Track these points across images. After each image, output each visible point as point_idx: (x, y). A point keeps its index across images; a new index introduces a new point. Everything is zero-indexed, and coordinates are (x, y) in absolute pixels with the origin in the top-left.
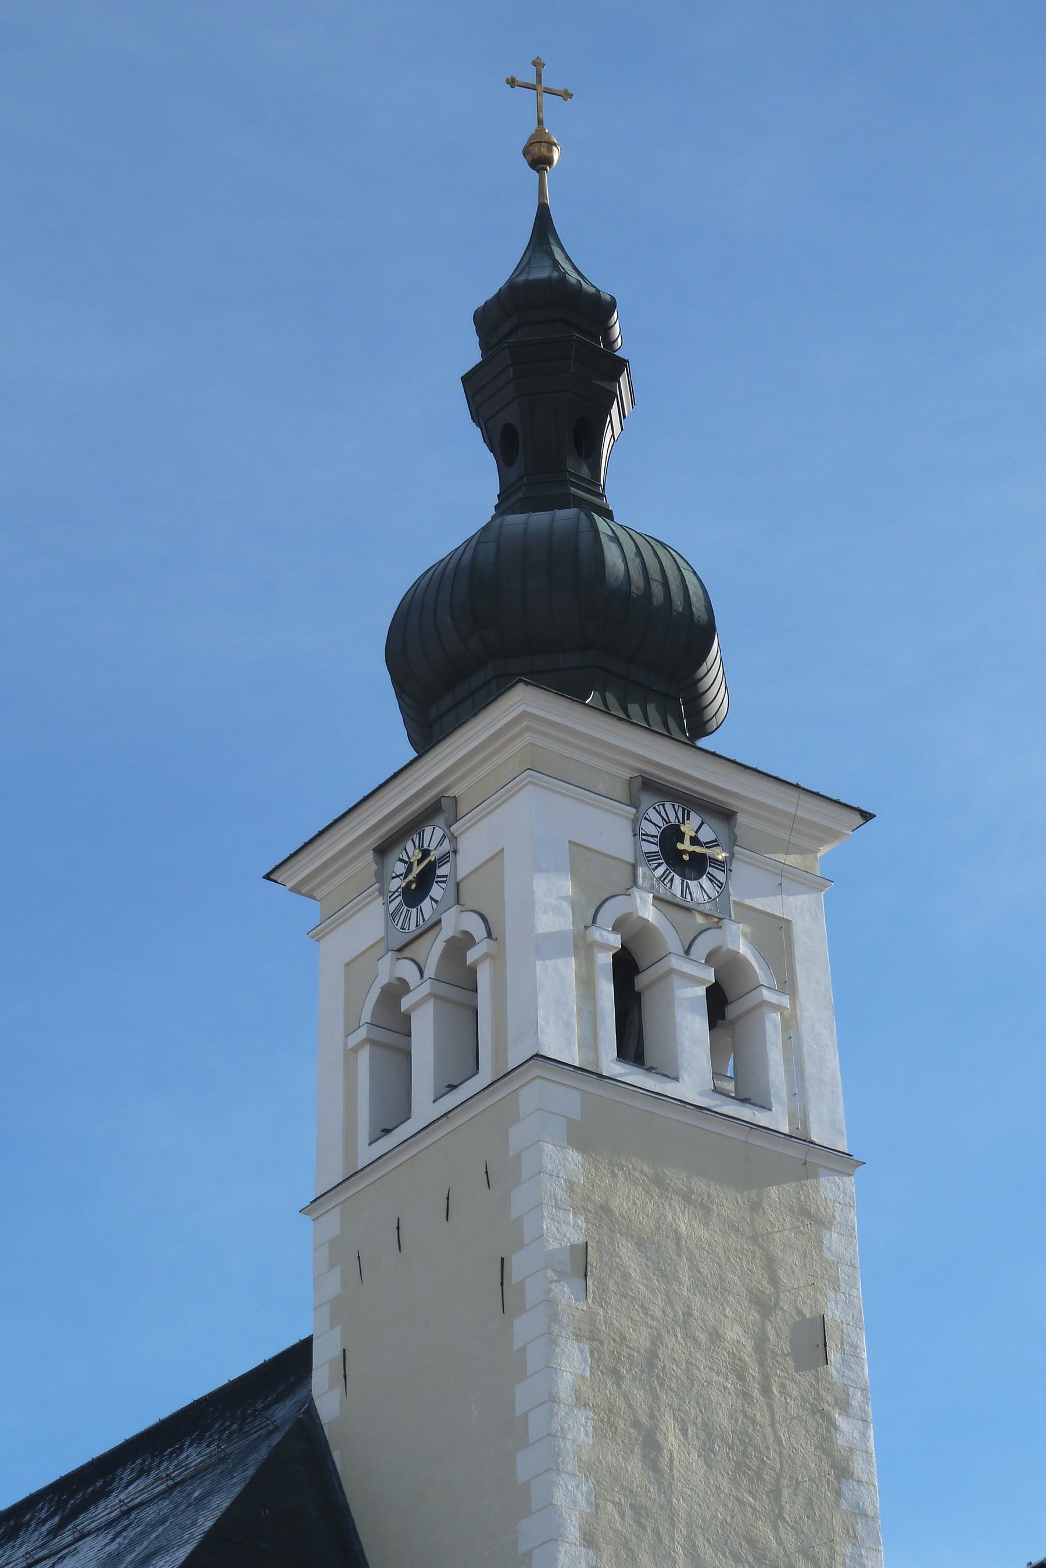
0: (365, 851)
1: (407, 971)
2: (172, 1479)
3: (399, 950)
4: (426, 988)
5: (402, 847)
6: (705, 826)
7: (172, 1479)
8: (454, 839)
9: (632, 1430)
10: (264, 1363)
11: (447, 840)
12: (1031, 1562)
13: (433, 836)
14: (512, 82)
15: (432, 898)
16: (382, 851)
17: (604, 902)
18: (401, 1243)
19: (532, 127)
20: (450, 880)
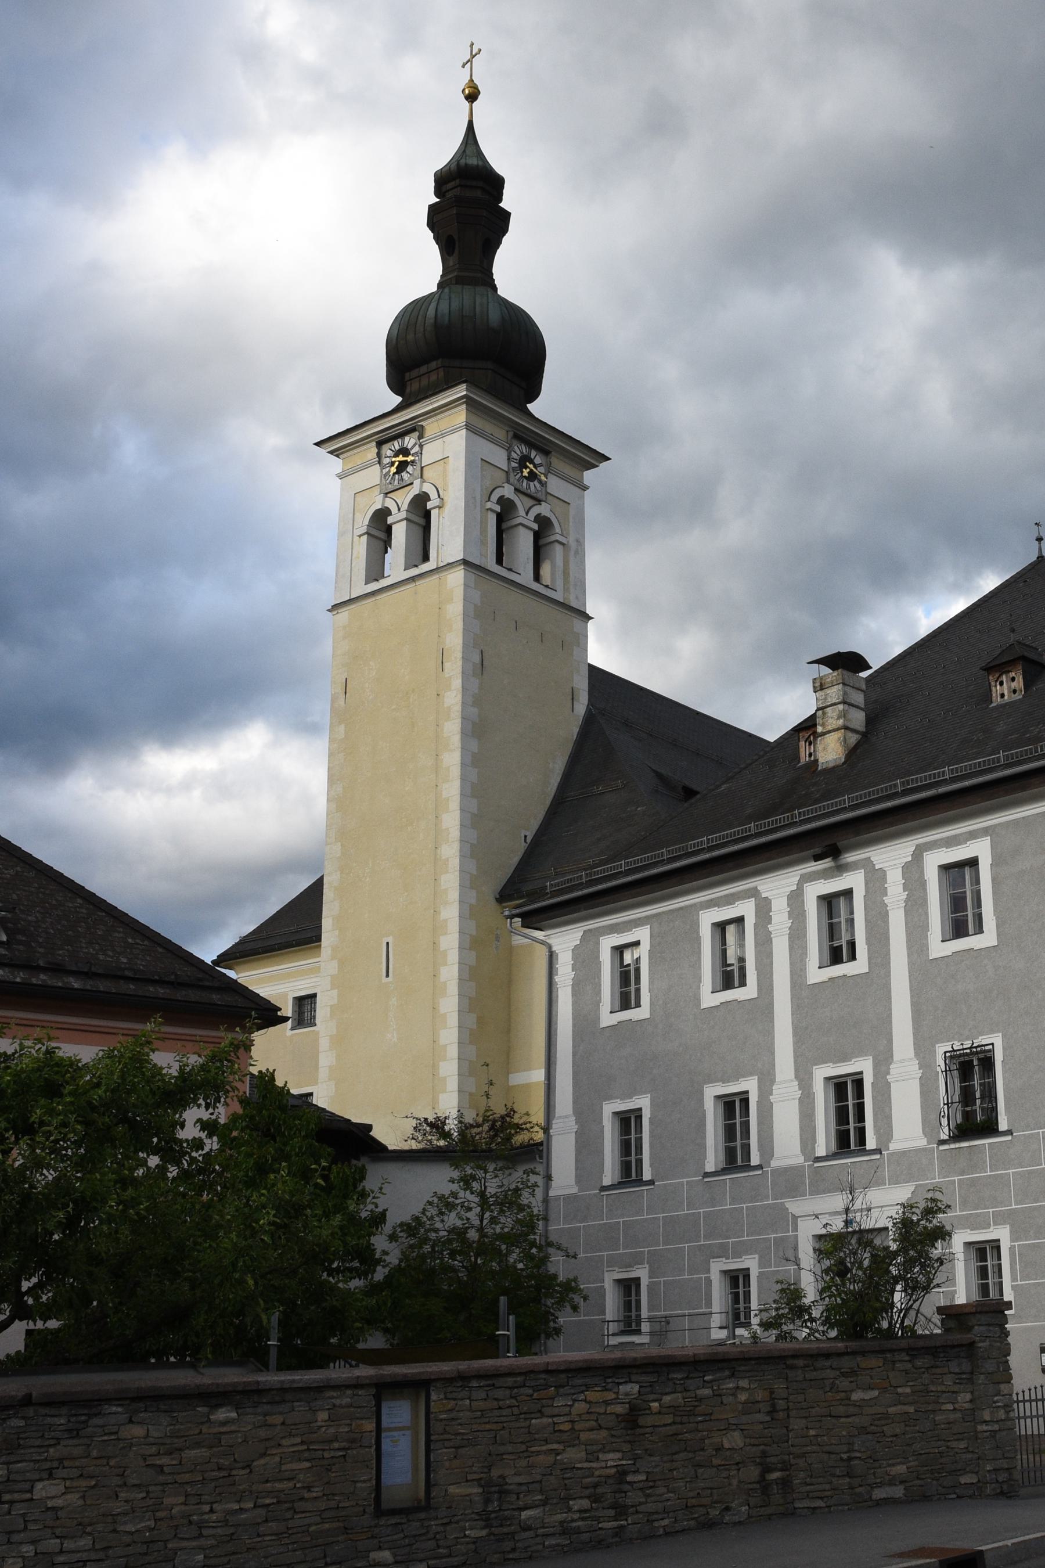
0: (373, 441)
1: (390, 504)
2: (830, 1483)
3: (387, 494)
4: (403, 515)
5: (391, 443)
6: (537, 456)
7: (830, 1483)
8: (421, 446)
9: (161, 1477)
10: (240, 940)
11: (417, 446)
12: (30, 1395)
13: (409, 441)
14: (472, 44)
15: (407, 472)
16: (380, 444)
17: (494, 490)
18: (380, 597)
19: (473, 105)
20: (418, 465)
